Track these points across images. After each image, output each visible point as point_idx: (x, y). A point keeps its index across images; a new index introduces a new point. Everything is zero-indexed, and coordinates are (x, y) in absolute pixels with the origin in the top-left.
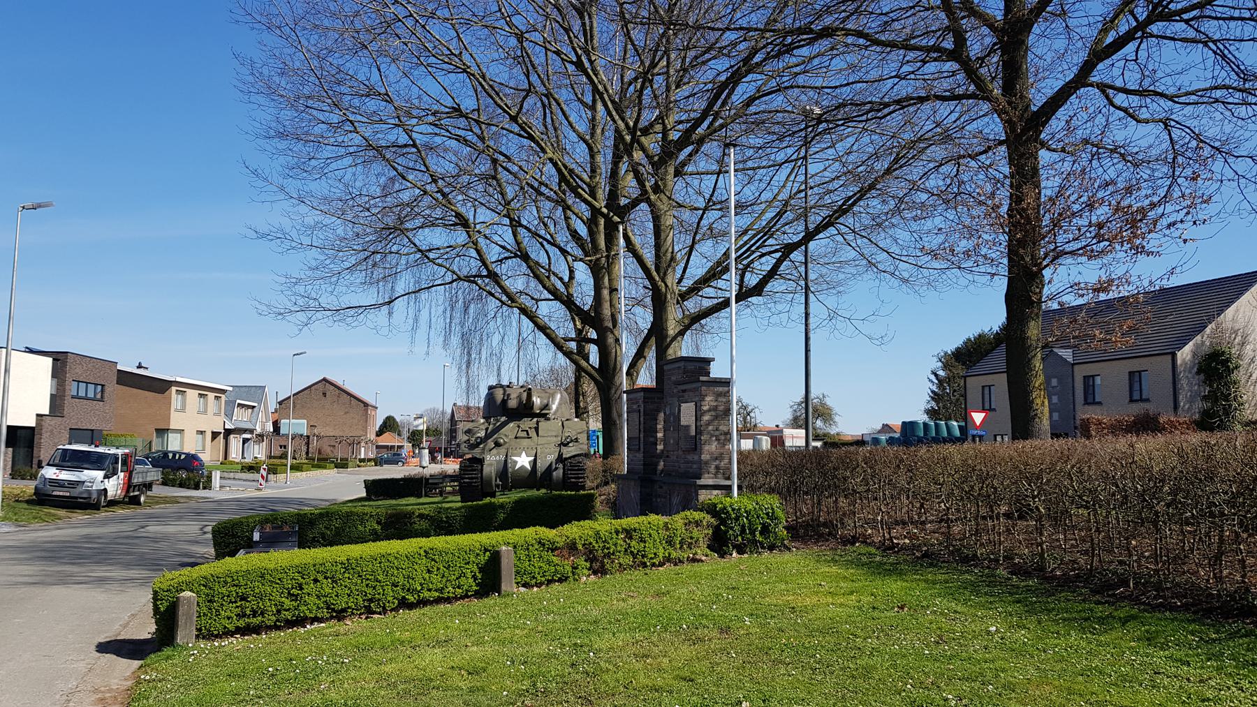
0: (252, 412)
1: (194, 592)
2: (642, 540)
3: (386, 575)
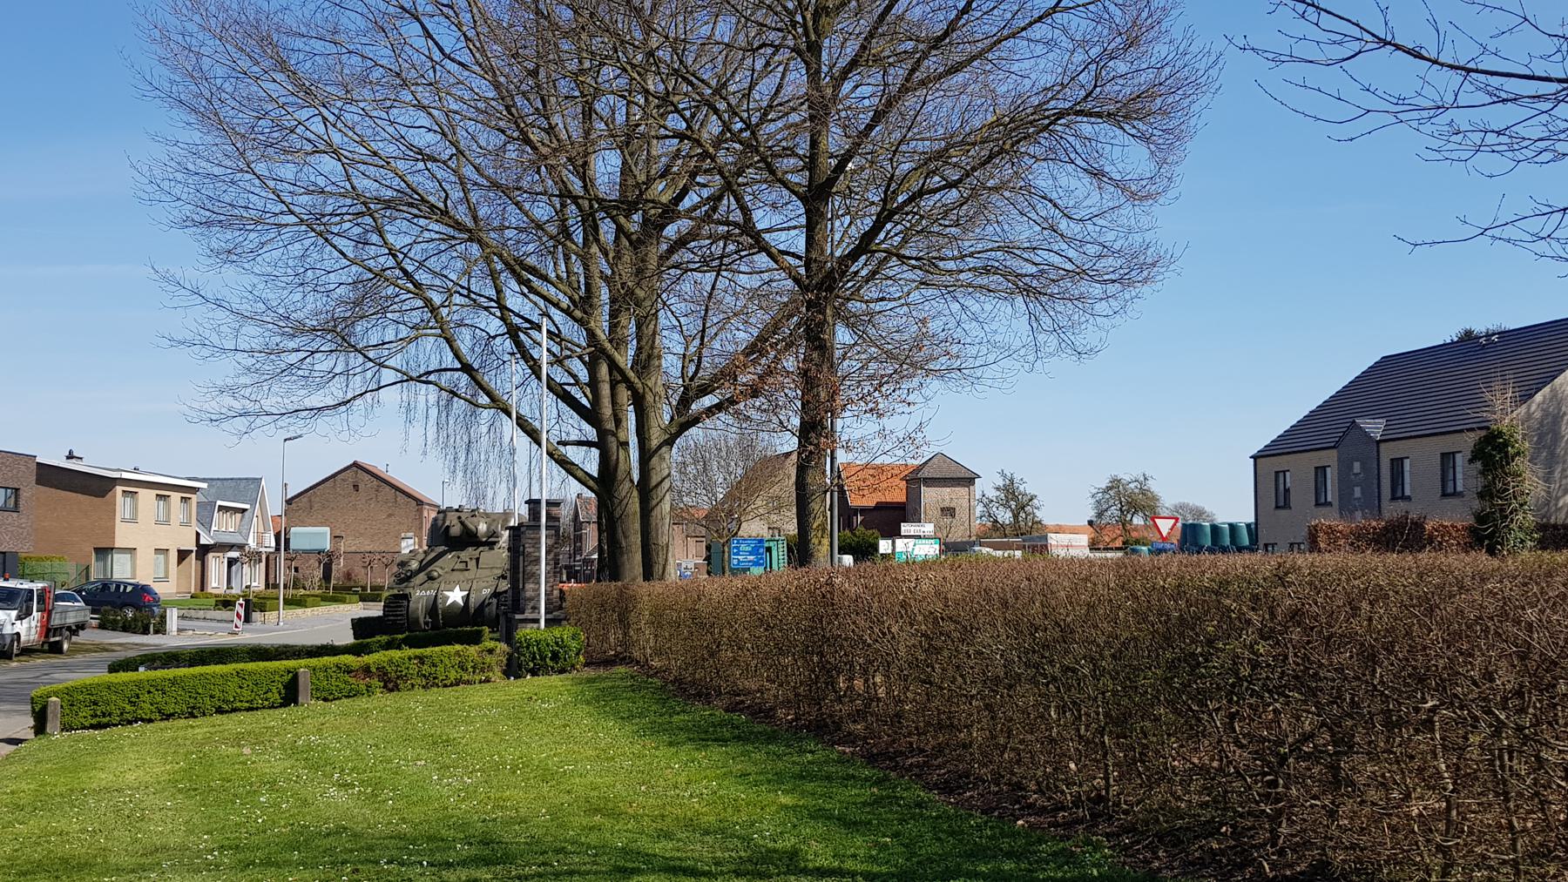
0: (243, 517)
2: (435, 665)
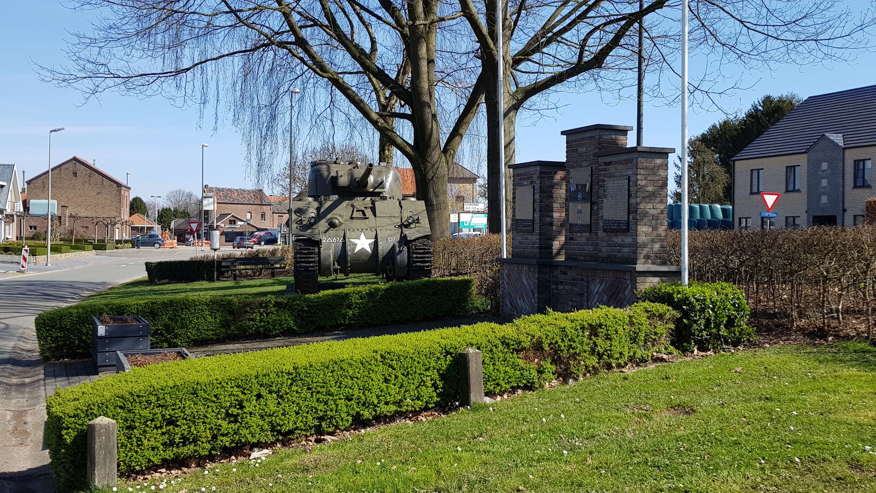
1: (109, 417)
2: (608, 338)
3: (340, 387)
